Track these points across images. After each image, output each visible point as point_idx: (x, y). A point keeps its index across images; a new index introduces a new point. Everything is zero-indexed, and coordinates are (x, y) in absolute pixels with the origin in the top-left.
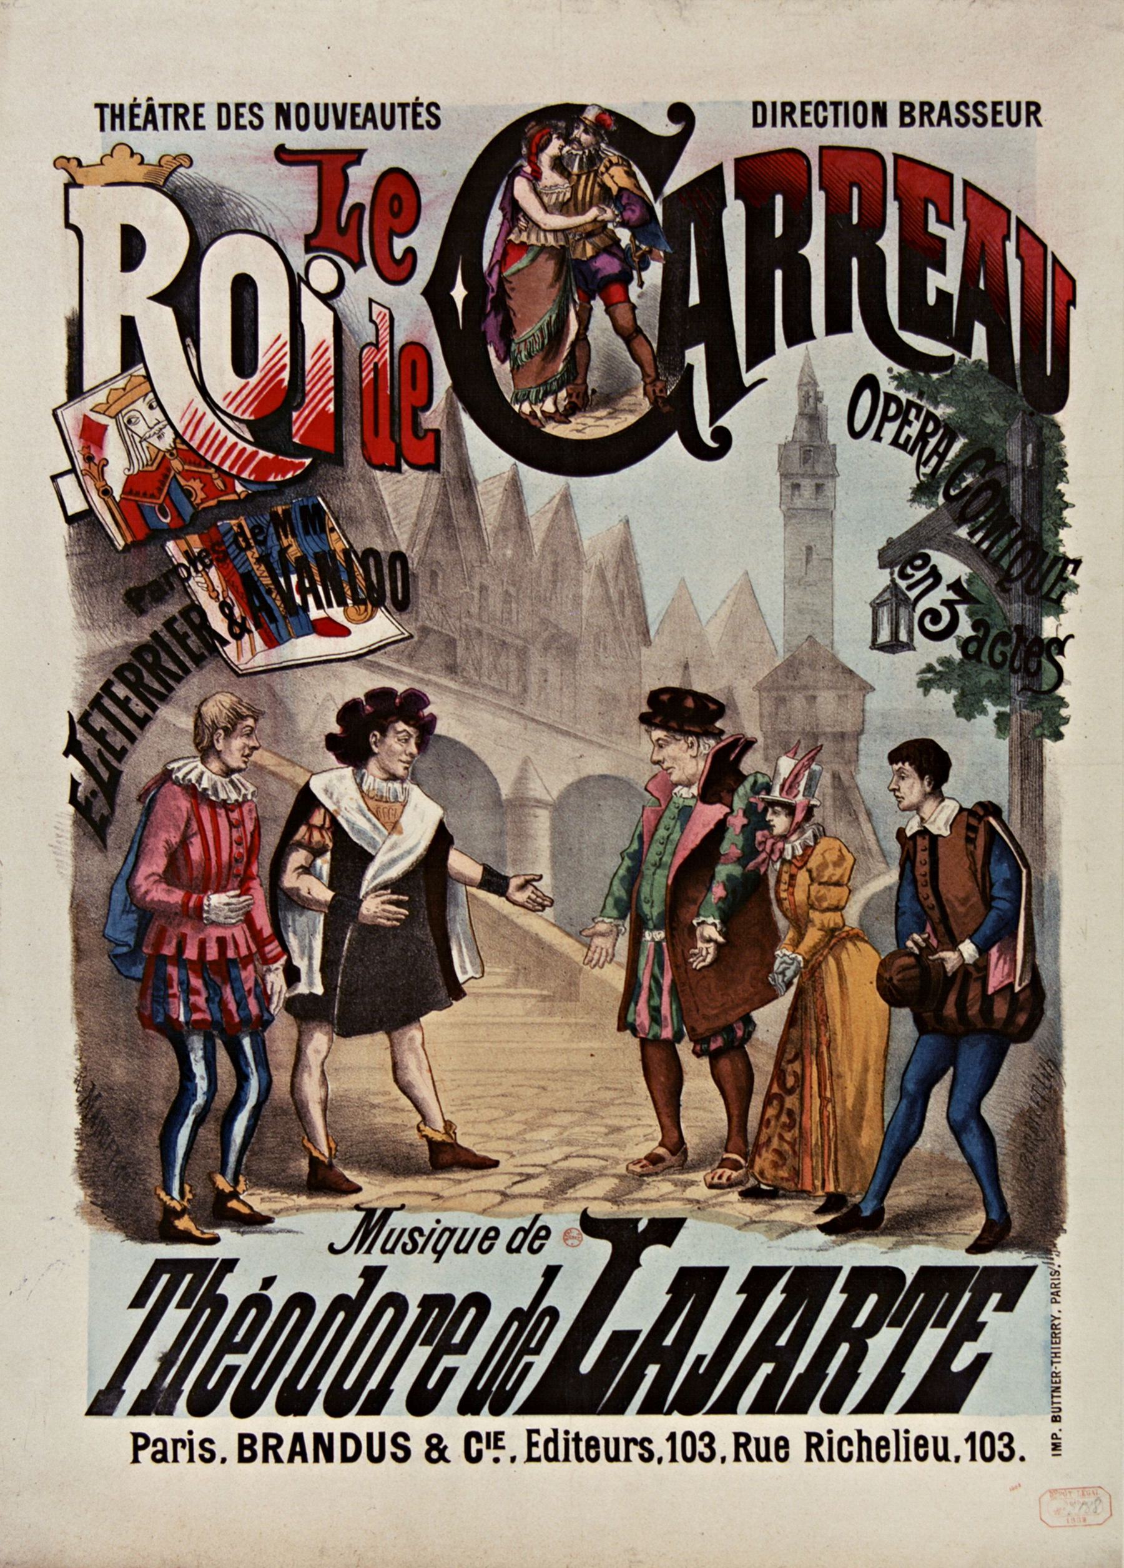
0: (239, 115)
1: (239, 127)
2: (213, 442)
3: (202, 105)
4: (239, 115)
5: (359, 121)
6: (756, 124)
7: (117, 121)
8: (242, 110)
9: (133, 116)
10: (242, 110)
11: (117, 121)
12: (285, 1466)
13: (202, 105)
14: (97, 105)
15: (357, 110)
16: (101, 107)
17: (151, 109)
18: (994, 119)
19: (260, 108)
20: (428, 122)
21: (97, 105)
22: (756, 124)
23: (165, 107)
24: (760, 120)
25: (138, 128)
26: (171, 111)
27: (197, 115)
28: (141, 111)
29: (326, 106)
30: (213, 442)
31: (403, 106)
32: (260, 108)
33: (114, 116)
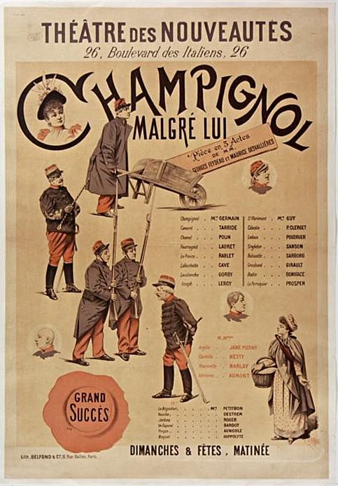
0: (142, 34)
1: (142, 40)
2: (59, 239)
3: (124, 24)
4: (142, 34)
5: (76, 37)
6: (132, 454)
7: (60, 36)
8: (143, 32)
9: (72, 32)
10: (143, 32)
11: (60, 36)
12: (240, 456)
13: (124, 24)
14: (43, 24)
15: (75, 28)
16: (47, 25)
17: (85, 26)
18: (141, 38)
19: (154, 31)
20: (149, 39)
21: (43, 24)
22: (132, 454)
23: (97, 25)
24: (134, 39)
25: (76, 41)
26: (102, 28)
27: (120, 32)
28: (78, 29)
29: (200, 24)
30: (59, 239)
31: (261, 24)
32: (154, 31)
33: (57, 32)
